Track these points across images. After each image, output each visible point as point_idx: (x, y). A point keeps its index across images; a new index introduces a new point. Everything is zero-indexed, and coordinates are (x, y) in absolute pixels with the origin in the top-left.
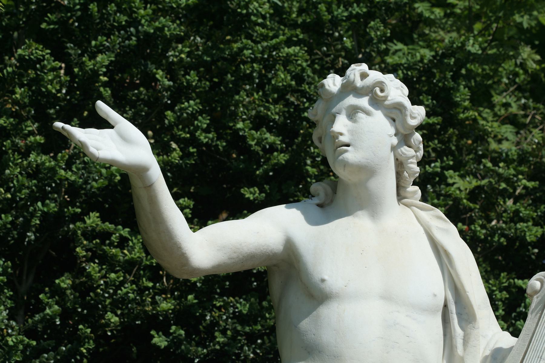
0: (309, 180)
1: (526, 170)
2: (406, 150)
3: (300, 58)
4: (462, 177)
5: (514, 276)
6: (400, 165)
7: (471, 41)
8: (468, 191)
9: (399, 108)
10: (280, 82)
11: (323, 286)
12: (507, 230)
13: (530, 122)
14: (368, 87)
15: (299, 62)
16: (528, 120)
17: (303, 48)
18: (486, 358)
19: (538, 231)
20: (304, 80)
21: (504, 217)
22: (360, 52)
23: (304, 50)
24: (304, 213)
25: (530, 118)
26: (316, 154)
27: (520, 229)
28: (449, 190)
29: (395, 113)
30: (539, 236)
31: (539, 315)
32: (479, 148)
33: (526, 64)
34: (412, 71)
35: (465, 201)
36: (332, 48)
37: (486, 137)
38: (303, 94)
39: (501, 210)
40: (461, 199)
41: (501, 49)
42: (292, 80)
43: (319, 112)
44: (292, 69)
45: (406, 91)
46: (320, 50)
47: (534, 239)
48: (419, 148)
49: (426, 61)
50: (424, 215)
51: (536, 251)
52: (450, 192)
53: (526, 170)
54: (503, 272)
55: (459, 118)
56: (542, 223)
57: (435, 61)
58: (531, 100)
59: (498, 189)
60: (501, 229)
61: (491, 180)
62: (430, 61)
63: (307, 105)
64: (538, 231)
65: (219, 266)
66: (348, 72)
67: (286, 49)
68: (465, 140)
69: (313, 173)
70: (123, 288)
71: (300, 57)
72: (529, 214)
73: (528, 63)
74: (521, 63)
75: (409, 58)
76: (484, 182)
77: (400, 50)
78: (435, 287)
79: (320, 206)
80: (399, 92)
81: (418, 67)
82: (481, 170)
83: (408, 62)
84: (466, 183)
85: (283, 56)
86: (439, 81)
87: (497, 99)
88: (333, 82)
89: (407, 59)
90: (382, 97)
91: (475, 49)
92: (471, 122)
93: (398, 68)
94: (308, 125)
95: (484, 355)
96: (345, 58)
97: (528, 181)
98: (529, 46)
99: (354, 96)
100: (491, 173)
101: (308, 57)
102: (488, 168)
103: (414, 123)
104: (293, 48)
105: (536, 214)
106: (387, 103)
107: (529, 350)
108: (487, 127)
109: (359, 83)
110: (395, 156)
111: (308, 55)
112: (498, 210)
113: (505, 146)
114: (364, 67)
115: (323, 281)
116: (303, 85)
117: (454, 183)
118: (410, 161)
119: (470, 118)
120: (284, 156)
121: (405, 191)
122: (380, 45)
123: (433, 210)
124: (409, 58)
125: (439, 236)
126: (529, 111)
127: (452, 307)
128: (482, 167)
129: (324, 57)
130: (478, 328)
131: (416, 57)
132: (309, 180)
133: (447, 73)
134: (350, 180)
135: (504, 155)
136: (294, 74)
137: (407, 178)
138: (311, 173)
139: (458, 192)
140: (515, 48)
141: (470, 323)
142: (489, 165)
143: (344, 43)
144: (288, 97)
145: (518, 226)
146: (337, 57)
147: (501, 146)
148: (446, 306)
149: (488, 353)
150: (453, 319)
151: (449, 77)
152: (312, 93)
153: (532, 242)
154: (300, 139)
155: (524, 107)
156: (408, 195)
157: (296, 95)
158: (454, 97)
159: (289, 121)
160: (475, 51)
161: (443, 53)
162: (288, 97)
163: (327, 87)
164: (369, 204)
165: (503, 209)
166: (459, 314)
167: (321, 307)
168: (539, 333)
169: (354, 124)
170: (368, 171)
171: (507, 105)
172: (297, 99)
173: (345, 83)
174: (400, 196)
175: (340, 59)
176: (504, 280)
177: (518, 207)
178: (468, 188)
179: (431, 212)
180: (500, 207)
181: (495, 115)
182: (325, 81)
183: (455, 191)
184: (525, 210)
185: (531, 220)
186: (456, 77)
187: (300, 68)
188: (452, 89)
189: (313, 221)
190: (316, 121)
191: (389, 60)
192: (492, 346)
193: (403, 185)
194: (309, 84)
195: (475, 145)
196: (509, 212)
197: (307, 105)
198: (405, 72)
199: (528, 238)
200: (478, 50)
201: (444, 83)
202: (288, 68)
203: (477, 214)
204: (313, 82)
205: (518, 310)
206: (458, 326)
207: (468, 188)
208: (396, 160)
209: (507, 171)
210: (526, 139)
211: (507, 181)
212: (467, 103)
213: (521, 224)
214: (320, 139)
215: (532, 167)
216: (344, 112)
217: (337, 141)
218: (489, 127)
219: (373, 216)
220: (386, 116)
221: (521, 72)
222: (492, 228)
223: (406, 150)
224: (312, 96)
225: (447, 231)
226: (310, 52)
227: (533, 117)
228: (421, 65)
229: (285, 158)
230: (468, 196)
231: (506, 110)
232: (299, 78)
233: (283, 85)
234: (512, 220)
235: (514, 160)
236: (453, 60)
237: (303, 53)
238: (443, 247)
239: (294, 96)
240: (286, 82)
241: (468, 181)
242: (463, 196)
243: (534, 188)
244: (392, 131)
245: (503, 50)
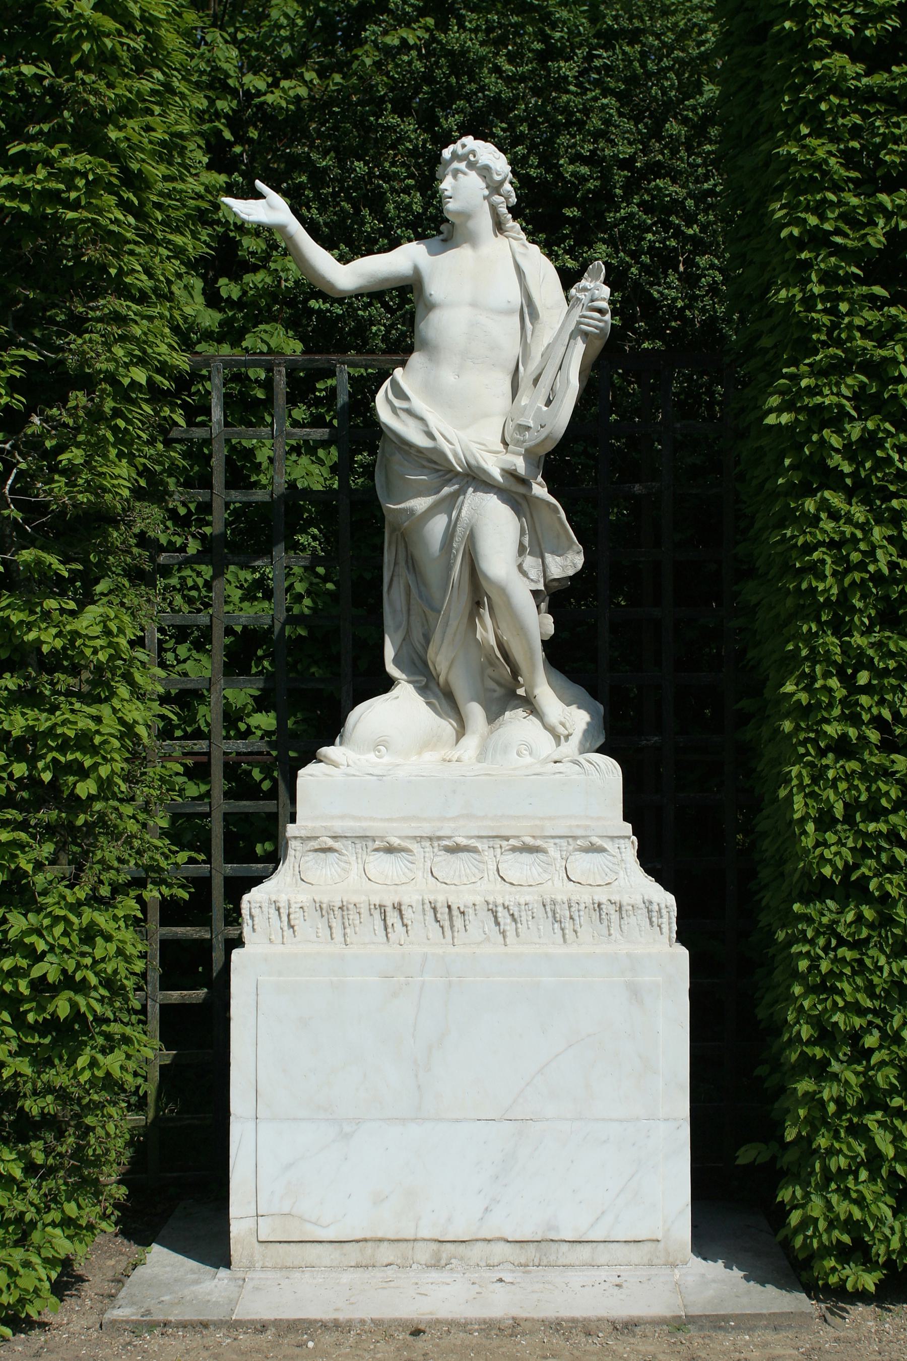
65: (361, 288)
70: (848, 535)
127: (526, 310)
164: (471, 239)
166: (530, 314)
170: (466, 215)
189: (432, 252)
220: (479, 175)
223: (497, 199)
244: (484, 185)
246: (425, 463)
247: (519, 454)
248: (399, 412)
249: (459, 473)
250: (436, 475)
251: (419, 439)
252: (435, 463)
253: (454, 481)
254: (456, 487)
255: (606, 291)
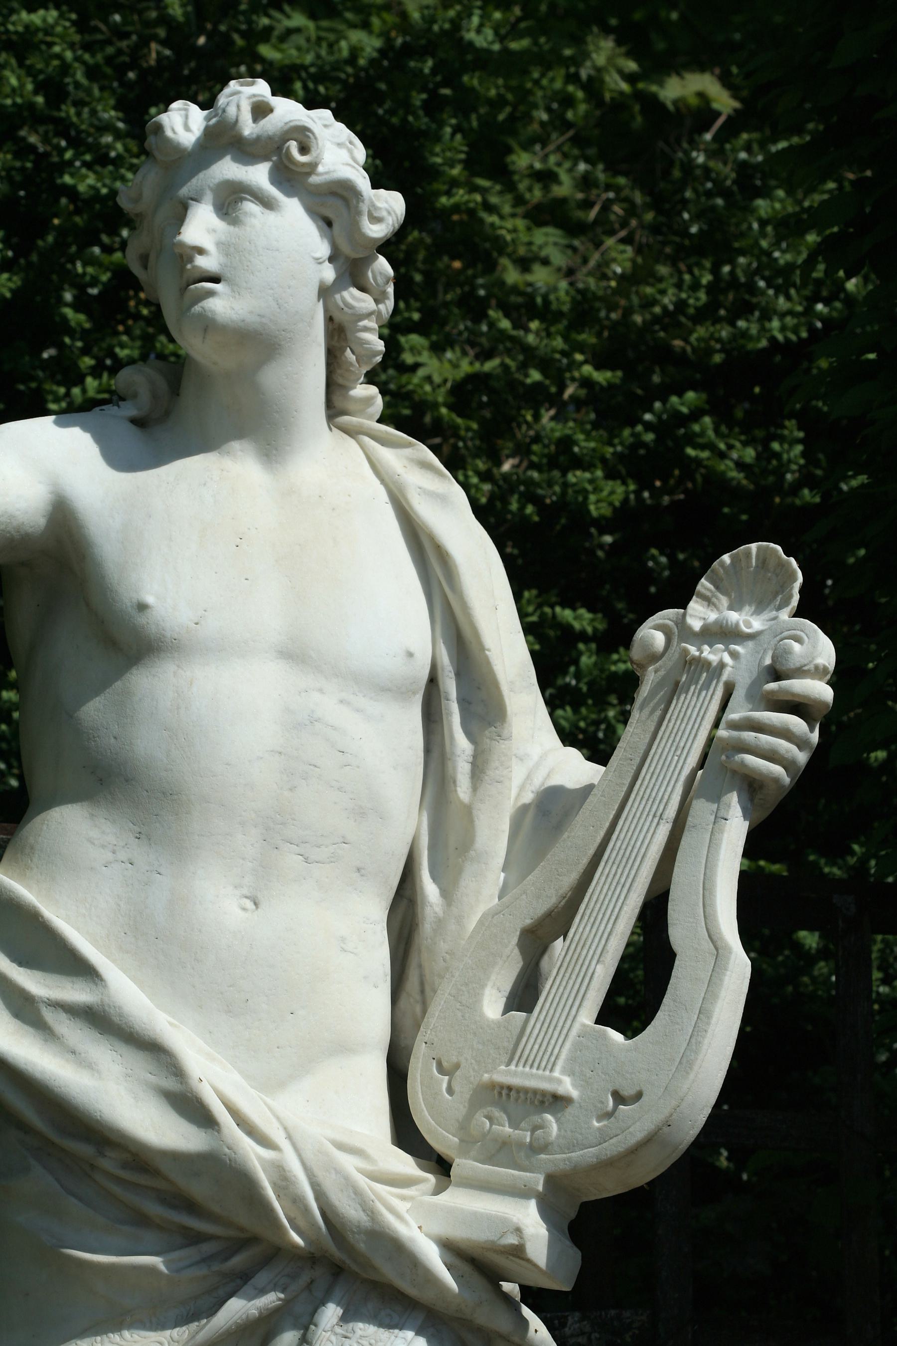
0: (67, 340)
1: (593, 340)
2: (353, 297)
3: (57, 40)
4: (437, 349)
5: (554, 599)
6: (338, 333)
7: (475, 20)
8: (449, 385)
9: (345, 194)
10: (7, 96)
11: (141, 620)
12: (544, 485)
13: (596, 222)
14: (270, 138)
15: (57, 49)
16: (593, 214)
17: (67, 15)
18: (524, 809)
19: (617, 491)
20: (67, 94)
21: (535, 454)
22: (201, 31)
23: (69, 20)
24: (100, 439)
25: (596, 209)
26: (88, 278)
27: (574, 485)
28: (408, 383)
29: (332, 206)
30: (617, 504)
31: (658, 713)
32: (480, 281)
33: (602, 82)
34: (328, 84)
35: (444, 411)
36: (136, 17)
37: (495, 254)
38: (63, 128)
39: (525, 436)
40: (435, 406)
41: (542, 40)
42: (36, 92)
43: (148, 193)
44: (40, 66)
45: (361, 153)
46: (106, 21)
47: (606, 511)
48: (384, 294)
49: (362, 62)
50: (389, 456)
51: (608, 539)
52: (410, 387)
53: (593, 340)
54: (529, 588)
55: (438, 205)
56: (623, 471)
57: (385, 63)
58: (600, 167)
59: (523, 384)
60: (530, 482)
61: (508, 361)
62: (372, 62)
63: (68, 155)
64: (617, 491)
66: (222, 100)
67: (24, 15)
68: (446, 259)
69: (79, 324)
71: (58, 36)
72: (594, 450)
73: (607, 79)
74: (590, 78)
75: (323, 52)
76: (490, 365)
77: (298, 30)
78: (404, 630)
79: (139, 423)
80: (344, 154)
81: (343, 76)
82: (482, 334)
83: (319, 62)
84: (447, 365)
85: (16, 33)
86: (392, 112)
87: (522, 160)
88: (183, 122)
89: (318, 56)
90: (304, 165)
91: (486, 39)
92: (465, 217)
93: (295, 76)
94: (72, 207)
95: (519, 804)
96: (164, 43)
97: (597, 368)
98: (612, 37)
99: (236, 159)
100: (508, 345)
101: (77, 38)
102: (502, 332)
103: (377, 231)
104: (41, 12)
105: (611, 450)
106: (314, 179)
107: (633, 796)
108: (503, 232)
109: (248, 128)
110: (326, 310)
111: (78, 32)
112: (519, 436)
113: (540, 276)
114: (262, 88)
115: (142, 607)
116: (63, 107)
117: (416, 366)
118: (361, 324)
119: (463, 207)
120: (10, 279)
121: (346, 397)
122: (254, 17)
123: (410, 445)
124: (323, 52)
125: (427, 512)
126: (595, 192)
127: (450, 686)
128: (484, 328)
129: (115, 39)
130: (509, 738)
131: (340, 50)
132: (67, 340)
133: (414, 94)
134: (215, 363)
135: (539, 300)
136: (41, 77)
137: (351, 364)
138: (73, 324)
139: (428, 388)
140: (578, 40)
141: (490, 724)
142: (505, 324)
143: (166, 7)
144: (23, 133)
145: (571, 478)
146: (144, 42)
147: (529, 278)
148: (433, 681)
149: (528, 797)
150: (450, 714)
151: (418, 103)
152: (83, 127)
153: (602, 517)
154: (50, 239)
155: (586, 182)
156: (351, 407)
157: (41, 129)
158: (427, 154)
159: (22, 193)
160: (485, 45)
161: (405, 44)
162: (23, 133)
163: (169, 133)
164: (258, 425)
165: (532, 433)
166: (464, 702)
167: (134, 671)
168: (657, 757)
169: (232, 228)
170: (260, 344)
171: (546, 177)
172: (46, 140)
173: (215, 125)
174: (335, 407)
175: (154, 46)
176: (530, 609)
177: (568, 432)
178: (450, 378)
179: (407, 451)
180: (524, 427)
181: (519, 201)
182: (164, 118)
183: (421, 386)
184: (586, 440)
185: (599, 465)
186: (433, 106)
187: (56, 63)
188: (423, 134)
189: (120, 459)
190: (137, 215)
191: (266, 51)
192: (539, 782)
193: (340, 381)
194: (79, 104)
195: (470, 272)
196: (546, 441)
197: (68, 155)
198: (311, 85)
199: (592, 508)
200: (492, 43)
201: (404, 120)
202: (28, 62)
203: (470, 444)
204: (87, 99)
205: (560, 682)
206: (461, 731)
207: (450, 378)
208: (329, 320)
209: (545, 341)
210: (585, 261)
211: (545, 365)
212: (456, 171)
213: (578, 473)
214: (144, 260)
215: (606, 334)
216: (209, 197)
217: (189, 266)
218: (509, 231)
219: (267, 455)
220: (311, 211)
221: (580, 94)
222: (506, 477)
223: (356, 299)
224: (83, 135)
225: (442, 499)
226: (81, 25)
227: (606, 207)
228: (350, 70)
229: (12, 285)
230: (451, 400)
231: (546, 189)
232: (54, 88)
233: (14, 104)
234: (552, 462)
235: (560, 314)
236: (430, 63)
237: (65, 28)
238: (432, 539)
239: (37, 132)
240: (22, 96)
241: (450, 361)
242: (440, 399)
243: (611, 386)
244: (323, 249)
245: (547, 42)
246: (154, 1209)
247: (520, 1193)
248: (49, 1015)
249: (293, 1253)
250: (191, 1253)
251: (150, 1124)
252: (191, 1206)
253: (262, 1278)
254: (271, 1299)
255: (822, 649)
